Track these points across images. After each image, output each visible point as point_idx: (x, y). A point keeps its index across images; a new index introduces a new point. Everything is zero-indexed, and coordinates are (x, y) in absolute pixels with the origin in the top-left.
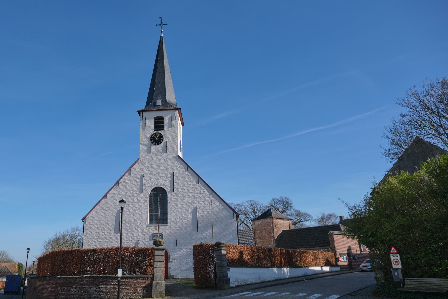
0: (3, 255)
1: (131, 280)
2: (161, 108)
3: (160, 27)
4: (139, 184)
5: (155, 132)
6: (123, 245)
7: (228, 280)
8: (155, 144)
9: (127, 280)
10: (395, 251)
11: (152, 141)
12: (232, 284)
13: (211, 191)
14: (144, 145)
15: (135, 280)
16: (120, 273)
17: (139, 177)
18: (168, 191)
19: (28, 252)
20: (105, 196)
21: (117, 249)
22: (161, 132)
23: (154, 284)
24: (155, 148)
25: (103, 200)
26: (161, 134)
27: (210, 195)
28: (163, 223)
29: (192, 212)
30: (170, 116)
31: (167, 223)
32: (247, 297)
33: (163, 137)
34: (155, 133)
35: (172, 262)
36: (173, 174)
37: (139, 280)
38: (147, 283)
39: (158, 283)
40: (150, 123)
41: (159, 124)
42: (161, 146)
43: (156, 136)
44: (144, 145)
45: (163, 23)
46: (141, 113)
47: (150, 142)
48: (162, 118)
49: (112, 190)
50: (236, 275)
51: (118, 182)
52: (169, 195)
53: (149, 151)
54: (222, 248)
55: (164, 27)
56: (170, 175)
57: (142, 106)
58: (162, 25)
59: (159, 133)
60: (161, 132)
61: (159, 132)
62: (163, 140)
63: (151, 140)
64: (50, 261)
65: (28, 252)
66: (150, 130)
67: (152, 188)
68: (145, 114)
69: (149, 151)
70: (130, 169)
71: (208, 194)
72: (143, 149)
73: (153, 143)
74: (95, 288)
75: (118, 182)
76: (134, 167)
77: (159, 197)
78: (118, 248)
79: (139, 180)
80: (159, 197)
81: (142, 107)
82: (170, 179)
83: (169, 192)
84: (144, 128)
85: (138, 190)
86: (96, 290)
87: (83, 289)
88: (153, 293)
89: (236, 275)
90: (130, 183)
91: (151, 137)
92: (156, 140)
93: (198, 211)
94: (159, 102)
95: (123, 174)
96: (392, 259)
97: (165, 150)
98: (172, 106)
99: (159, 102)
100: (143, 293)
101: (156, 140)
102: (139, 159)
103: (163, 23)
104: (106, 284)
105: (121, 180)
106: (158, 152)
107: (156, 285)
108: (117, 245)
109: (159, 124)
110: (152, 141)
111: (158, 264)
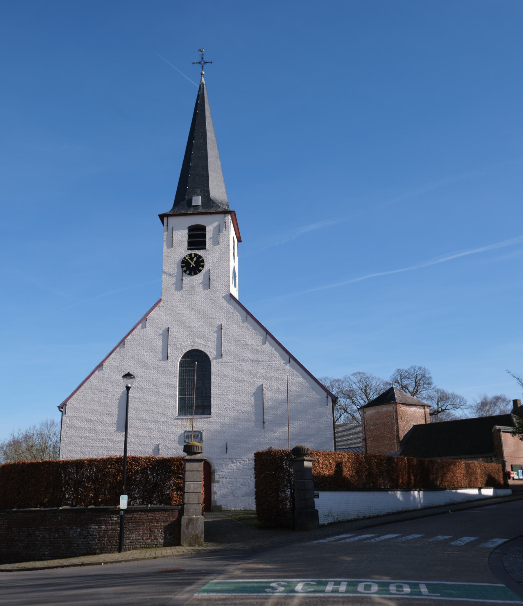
1: (144, 515)
2: (200, 210)
3: (199, 66)
4: (160, 344)
5: (190, 252)
6: (131, 453)
7: (315, 514)
8: (190, 274)
9: (137, 516)
11: (185, 269)
12: (322, 521)
13: (288, 357)
14: (170, 275)
15: (150, 515)
16: (124, 502)
17: (161, 332)
18: (211, 356)
19: (128, 388)
20: (100, 366)
21: (118, 460)
23: (184, 520)
24: (188, 280)
25: (96, 373)
26: (200, 257)
27: (286, 364)
28: (203, 413)
29: (254, 394)
30: (215, 224)
33: (203, 261)
34: (190, 255)
35: (218, 482)
36: (221, 328)
37: (158, 515)
38: (172, 519)
39: (190, 520)
40: (181, 237)
41: (197, 238)
42: (199, 277)
43: (192, 259)
44: (170, 275)
45: (205, 59)
46: (165, 219)
49: (113, 354)
50: (329, 504)
51: (122, 343)
52: (214, 364)
53: (179, 286)
54: (305, 458)
56: (215, 329)
57: (168, 207)
58: (202, 63)
59: (196, 255)
60: (201, 253)
61: (197, 252)
62: (203, 266)
63: (182, 267)
65: (128, 388)
66: (181, 248)
67: (185, 351)
68: (172, 221)
69: (179, 286)
70: (144, 319)
71: (283, 361)
72: (168, 282)
73: (185, 272)
74: (79, 530)
75: (122, 343)
76: (152, 314)
78: (120, 458)
79: (161, 338)
82: (216, 335)
83: (215, 358)
84: (171, 245)
85: (160, 355)
86: (80, 533)
88: (183, 537)
89: (329, 504)
90: (146, 339)
91: (183, 262)
92: (192, 266)
93: (266, 392)
94: (197, 200)
97: (207, 284)
98: (219, 207)
99: (197, 200)
100: (165, 538)
101: (192, 266)
102: (160, 300)
103: (205, 59)
104: (99, 523)
105: (130, 337)
106: (194, 288)
107: (188, 523)
108: (120, 453)
109: (197, 238)
110: (185, 269)
111: (192, 485)
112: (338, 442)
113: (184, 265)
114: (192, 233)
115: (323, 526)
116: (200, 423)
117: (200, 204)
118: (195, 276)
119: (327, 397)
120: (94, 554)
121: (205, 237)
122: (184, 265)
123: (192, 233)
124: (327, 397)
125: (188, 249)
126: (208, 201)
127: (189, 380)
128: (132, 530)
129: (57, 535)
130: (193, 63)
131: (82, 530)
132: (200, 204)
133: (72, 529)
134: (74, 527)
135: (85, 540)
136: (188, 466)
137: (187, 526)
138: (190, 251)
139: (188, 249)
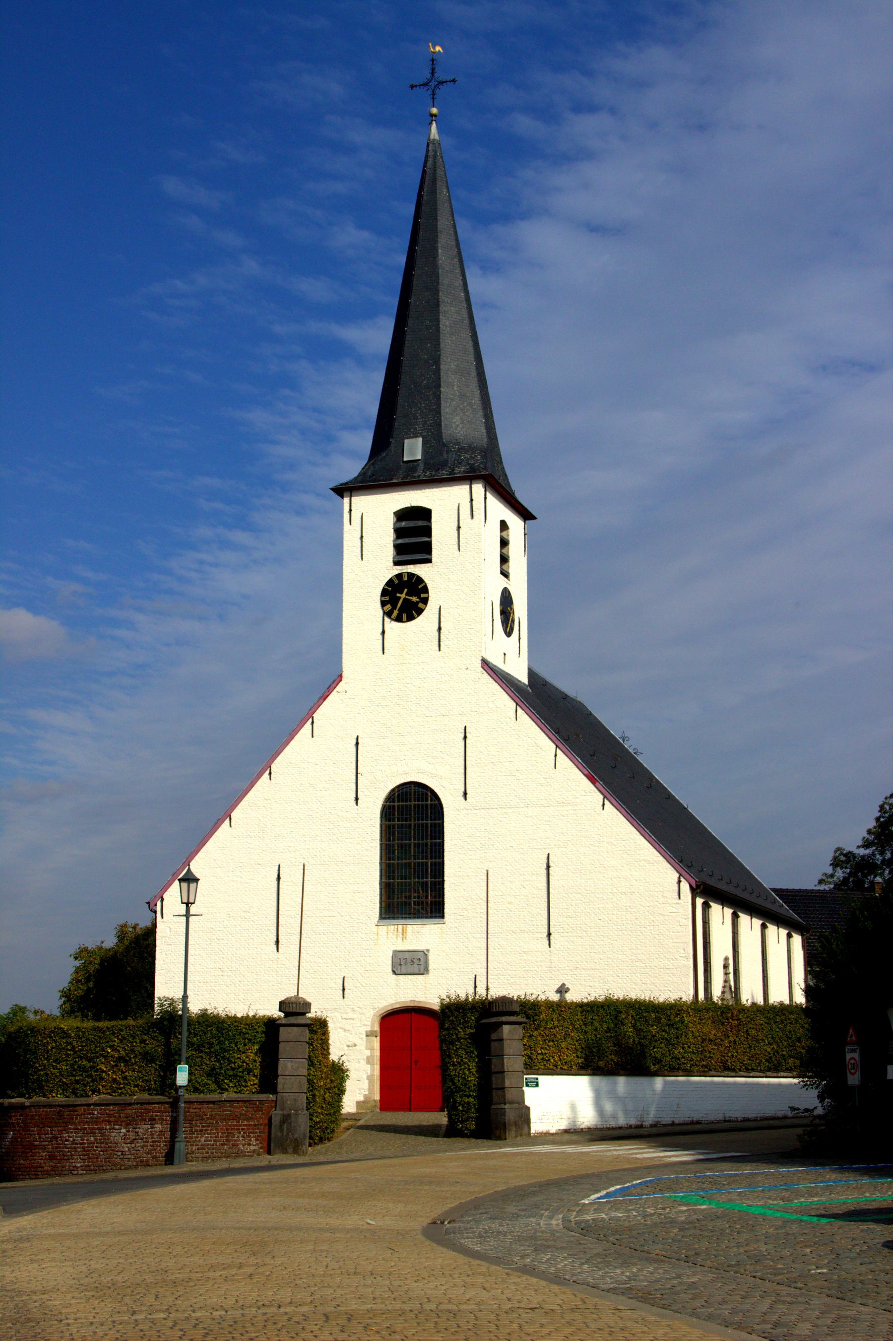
0: (78, 981)
3: (425, 93)
8: (399, 619)
10: (854, 1038)
21: (549, 1004)
22: (418, 570)
31: (443, 917)
32: (637, 1159)
41: (413, 535)
42: (426, 620)
45: (440, 75)
47: (380, 612)
48: (424, 514)
55: (442, 91)
59: (411, 575)
60: (418, 570)
63: (383, 604)
64: (551, 1217)
73: (388, 614)
74: (124, 1130)
77: (413, 832)
80: (413, 832)
81: (352, 469)
86: (125, 1135)
87: (92, 1132)
94: (414, 449)
95: (437, 616)
96: (848, 1056)
103: (440, 75)
111: (289, 1064)
112: (289, 1029)
113: (387, 598)
114: (403, 524)
115: (546, 1138)
116: (418, 934)
117: (419, 457)
118: (421, 616)
119: (679, 882)
120: (17, 1180)
121: (430, 535)
122: (387, 598)
123: (403, 524)
124: (679, 882)
125: (396, 563)
126: (436, 444)
127: (401, 846)
128: (201, 1131)
129: (92, 1139)
130: (412, 87)
131: (128, 1131)
132: (419, 457)
133: (113, 1128)
134: (117, 1127)
135: (133, 1145)
136: (284, 1033)
137: (281, 1126)
138: (399, 567)
139: (396, 563)
